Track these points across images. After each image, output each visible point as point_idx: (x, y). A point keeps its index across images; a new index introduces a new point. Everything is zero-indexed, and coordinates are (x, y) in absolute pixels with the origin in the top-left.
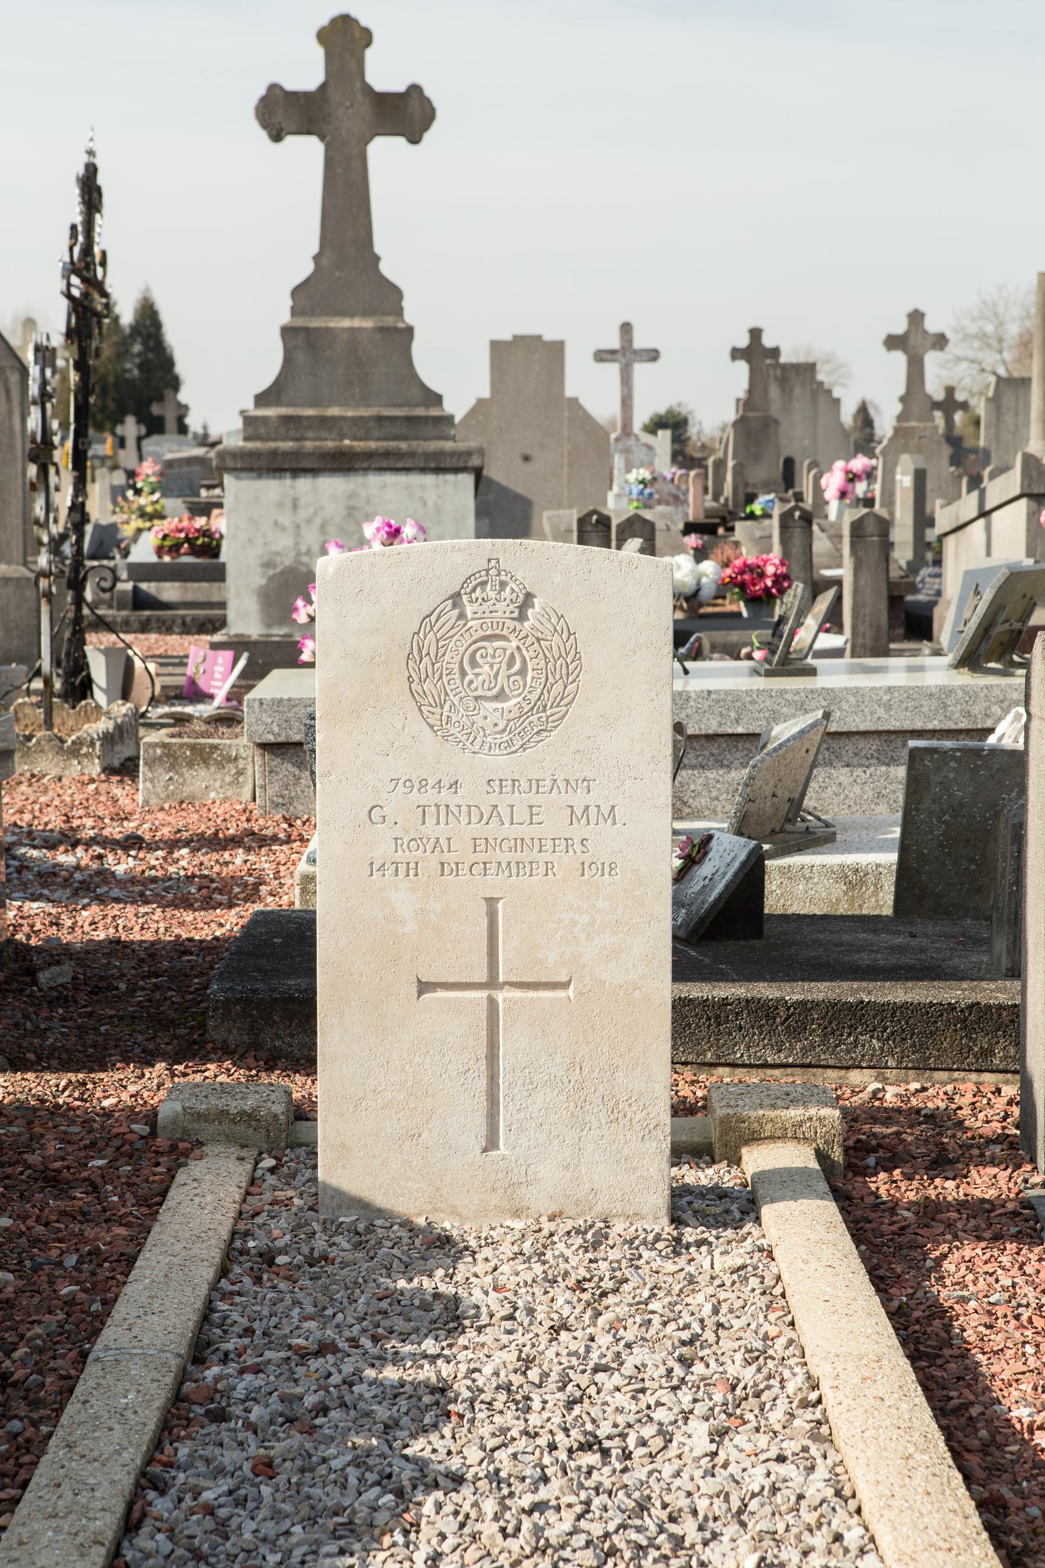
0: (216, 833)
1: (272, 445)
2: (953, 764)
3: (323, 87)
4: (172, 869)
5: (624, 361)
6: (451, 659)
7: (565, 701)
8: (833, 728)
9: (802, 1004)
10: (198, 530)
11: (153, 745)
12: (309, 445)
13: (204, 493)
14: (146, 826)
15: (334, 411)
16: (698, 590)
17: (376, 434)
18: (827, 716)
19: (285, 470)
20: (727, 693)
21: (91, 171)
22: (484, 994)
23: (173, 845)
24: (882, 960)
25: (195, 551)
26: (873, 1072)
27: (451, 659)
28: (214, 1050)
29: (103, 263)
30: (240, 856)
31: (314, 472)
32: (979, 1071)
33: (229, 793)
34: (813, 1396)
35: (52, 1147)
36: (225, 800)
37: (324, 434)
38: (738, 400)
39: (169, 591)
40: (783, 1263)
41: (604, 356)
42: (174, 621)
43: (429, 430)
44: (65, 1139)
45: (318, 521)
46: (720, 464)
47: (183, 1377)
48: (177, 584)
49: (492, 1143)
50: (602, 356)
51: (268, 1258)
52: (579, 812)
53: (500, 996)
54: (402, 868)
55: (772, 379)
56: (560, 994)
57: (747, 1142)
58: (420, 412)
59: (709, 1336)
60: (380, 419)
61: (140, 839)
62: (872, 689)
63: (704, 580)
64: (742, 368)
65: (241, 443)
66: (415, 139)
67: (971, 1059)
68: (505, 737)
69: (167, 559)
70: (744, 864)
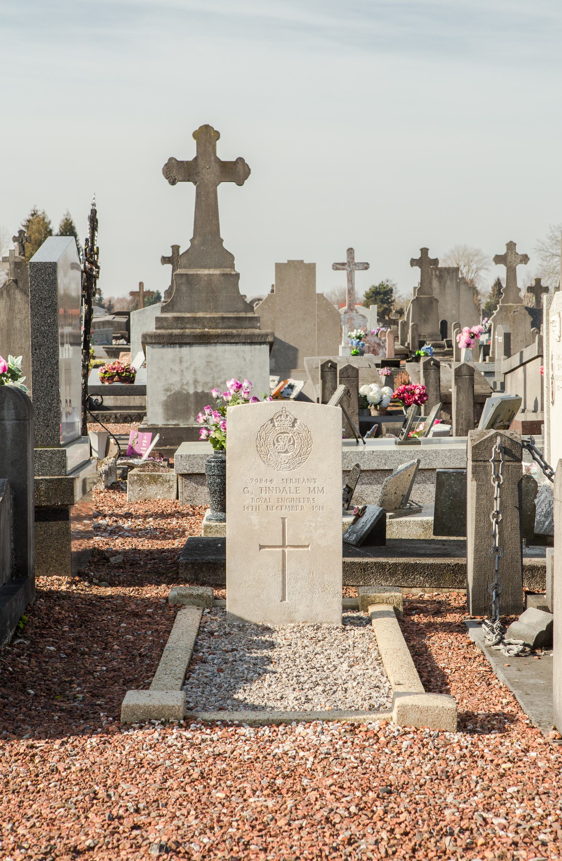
0: (163, 512)
1: (170, 331)
2: (453, 478)
3: (196, 159)
4: (147, 526)
5: (349, 269)
6: (270, 440)
7: (307, 453)
8: (420, 467)
9: (395, 564)
10: (123, 369)
11: (133, 475)
12: (188, 331)
13: (114, 342)
14: (132, 509)
15: (200, 315)
16: (381, 401)
17: (221, 326)
18: (419, 461)
19: (176, 344)
20: (381, 452)
21: (94, 212)
22: (281, 549)
23: (145, 517)
24: (428, 552)
25: (122, 380)
26: (421, 589)
27: (270, 440)
28: (182, 581)
29: (97, 254)
30: (174, 521)
31: (190, 344)
32: (458, 588)
33: (166, 496)
34: (379, 658)
35: (133, 607)
36: (163, 500)
37: (195, 326)
38: (415, 288)
39: (108, 401)
40: (376, 633)
41: (338, 266)
42: (110, 417)
43: (247, 323)
44: (137, 605)
45: (192, 368)
46: (405, 324)
47: (192, 655)
48: (112, 397)
49: (283, 599)
50: (337, 266)
51: (212, 633)
52: (312, 489)
53: (286, 550)
54: (254, 508)
55: (434, 277)
56: (306, 549)
57: (370, 604)
58: (242, 315)
59: (351, 648)
60: (223, 318)
61: (131, 514)
62: (442, 450)
63: (384, 396)
64: (417, 270)
65: (154, 331)
66: (240, 184)
67: (456, 584)
68: (288, 465)
69: (107, 384)
70: (378, 516)
